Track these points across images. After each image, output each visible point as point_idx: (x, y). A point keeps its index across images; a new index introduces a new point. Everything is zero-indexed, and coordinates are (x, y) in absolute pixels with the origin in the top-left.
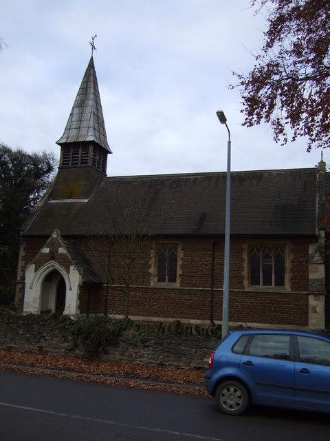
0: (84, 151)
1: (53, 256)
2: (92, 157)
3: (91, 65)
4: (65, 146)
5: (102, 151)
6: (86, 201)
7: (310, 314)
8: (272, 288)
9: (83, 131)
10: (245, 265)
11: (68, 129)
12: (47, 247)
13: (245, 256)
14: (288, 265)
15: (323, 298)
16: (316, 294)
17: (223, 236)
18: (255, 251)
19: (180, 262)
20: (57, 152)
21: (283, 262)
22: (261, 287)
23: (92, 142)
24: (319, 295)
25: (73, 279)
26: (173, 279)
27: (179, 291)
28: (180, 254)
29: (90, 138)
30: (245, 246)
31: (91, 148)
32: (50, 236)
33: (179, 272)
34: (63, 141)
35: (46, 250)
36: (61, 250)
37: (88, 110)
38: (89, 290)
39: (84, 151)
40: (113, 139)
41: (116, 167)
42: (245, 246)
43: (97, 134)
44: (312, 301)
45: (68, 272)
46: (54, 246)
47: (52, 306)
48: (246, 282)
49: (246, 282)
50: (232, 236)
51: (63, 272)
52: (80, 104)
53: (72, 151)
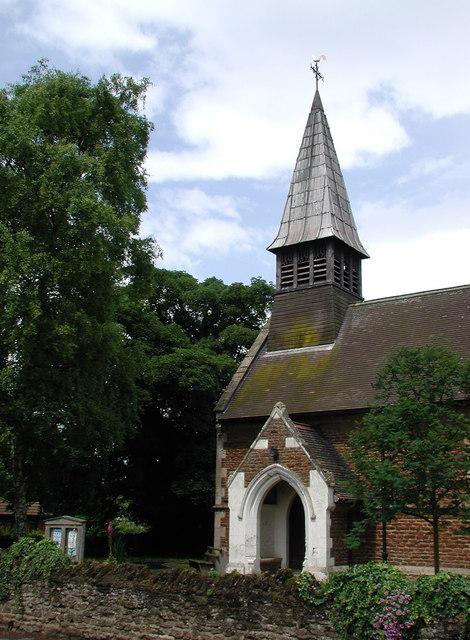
1: (275, 454)
2: (333, 266)
4: (283, 254)
5: (351, 257)
6: (330, 347)
9: (313, 222)
23: (332, 240)
25: (318, 497)
29: (328, 233)
31: (330, 254)
34: (278, 245)
36: (291, 443)
39: (324, 263)
45: (307, 483)
46: (277, 435)
51: (298, 486)
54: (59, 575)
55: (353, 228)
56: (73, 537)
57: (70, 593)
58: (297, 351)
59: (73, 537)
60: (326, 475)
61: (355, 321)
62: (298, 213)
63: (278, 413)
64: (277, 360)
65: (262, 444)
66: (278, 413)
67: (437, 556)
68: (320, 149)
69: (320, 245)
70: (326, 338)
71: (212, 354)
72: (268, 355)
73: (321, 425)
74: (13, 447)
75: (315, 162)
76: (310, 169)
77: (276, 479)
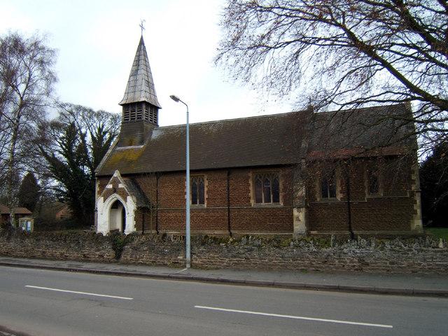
0: (139, 111)
1: (115, 190)
2: (145, 113)
3: (142, 39)
4: (125, 106)
5: (154, 108)
6: (142, 147)
7: (295, 223)
8: (272, 204)
9: (137, 94)
10: (251, 188)
11: (127, 93)
12: (111, 183)
13: (251, 182)
14: (281, 186)
15: (303, 210)
16: (299, 208)
17: (185, 171)
18: (258, 178)
19: (206, 189)
20: (119, 111)
21: (278, 185)
22: (263, 204)
23: (144, 102)
24: (299, 208)
25: (130, 205)
26: (202, 202)
27: (207, 210)
28: (206, 184)
29: (143, 99)
30: (250, 175)
31: (144, 106)
32: (111, 176)
33: (206, 196)
34: (123, 103)
35: (110, 186)
36: (121, 186)
37: (142, 71)
38: (142, 212)
39: (139, 111)
40: (162, 99)
41: (169, 117)
42: (250, 175)
43: (148, 95)
44: (295, 213)
45: (126, 201)
46: (116, 183)
47: (119, 226)
48: (252, 201)
49: (252, 201)
50: (191, 171)
51: (122, 201)
52: (134, 73)
53: (130, 109)
54: (25, 235)
55: (155, 96)
56: (29, 223)
57: (27, 241)
58: (129, 147)
59: (29, 223)
60: (135, 199)
61: (155, 135)
62: (132, 89)
63: (116, 174)
64: (122, 151)
65: (110, 186)
66: (116, 174)
67: (229, 227)
68: (142, 62)
69: (140, 104)
70: (142, 142)
71: (358, 102)
72: (118, 148)
73: (131, 177)
74: (39, 183)
75: (139, 68)
76: (137, 70)
77: (115, 199)
